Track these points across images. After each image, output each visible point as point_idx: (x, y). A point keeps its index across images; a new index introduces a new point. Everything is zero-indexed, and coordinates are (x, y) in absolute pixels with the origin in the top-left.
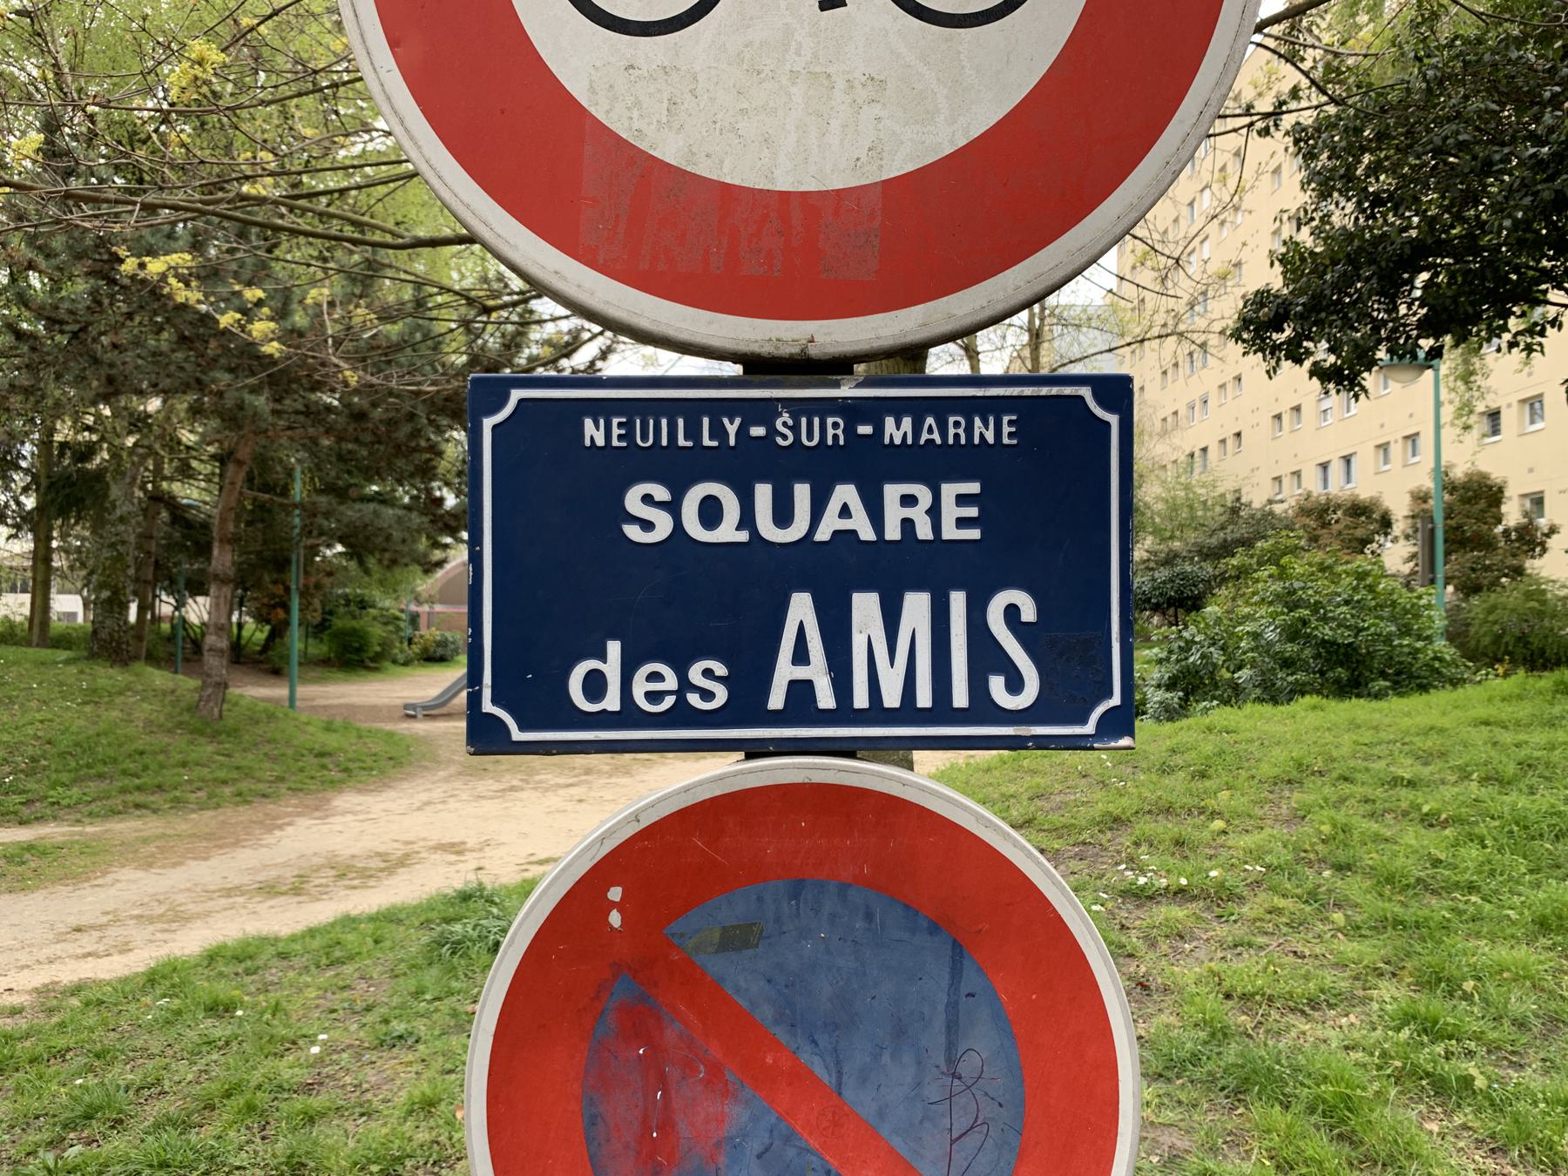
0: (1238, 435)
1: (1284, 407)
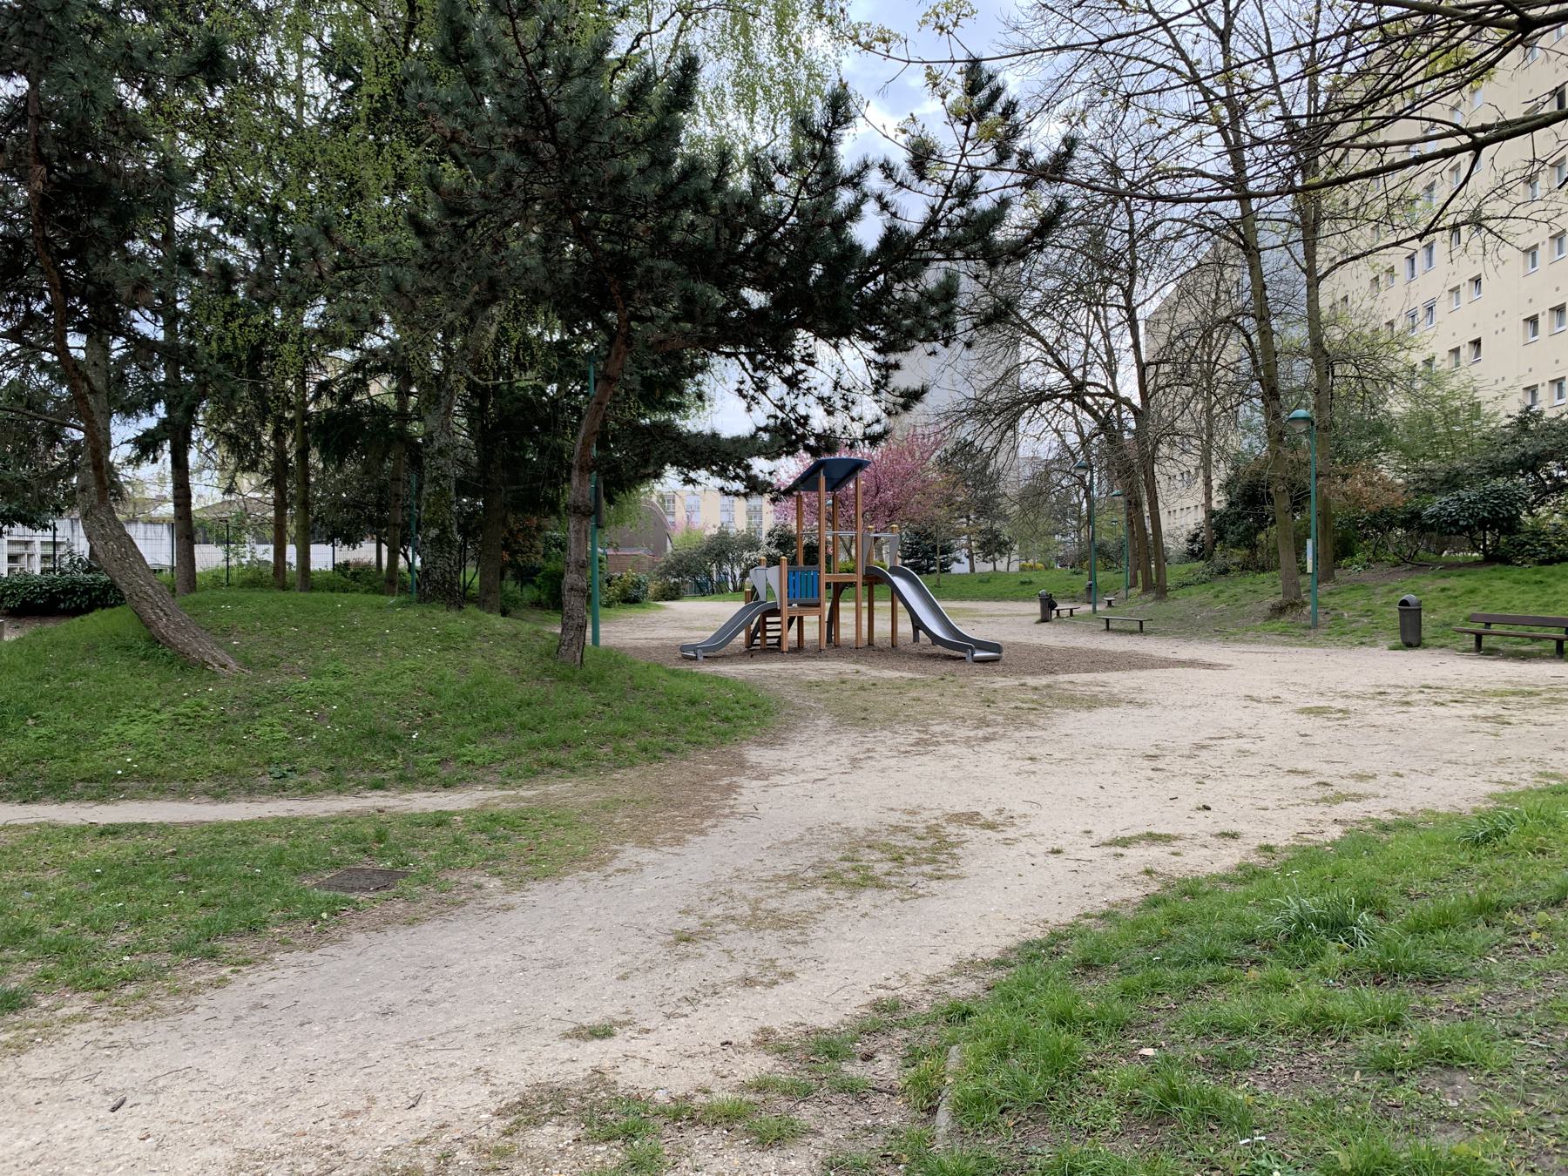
0: (1477, 343)
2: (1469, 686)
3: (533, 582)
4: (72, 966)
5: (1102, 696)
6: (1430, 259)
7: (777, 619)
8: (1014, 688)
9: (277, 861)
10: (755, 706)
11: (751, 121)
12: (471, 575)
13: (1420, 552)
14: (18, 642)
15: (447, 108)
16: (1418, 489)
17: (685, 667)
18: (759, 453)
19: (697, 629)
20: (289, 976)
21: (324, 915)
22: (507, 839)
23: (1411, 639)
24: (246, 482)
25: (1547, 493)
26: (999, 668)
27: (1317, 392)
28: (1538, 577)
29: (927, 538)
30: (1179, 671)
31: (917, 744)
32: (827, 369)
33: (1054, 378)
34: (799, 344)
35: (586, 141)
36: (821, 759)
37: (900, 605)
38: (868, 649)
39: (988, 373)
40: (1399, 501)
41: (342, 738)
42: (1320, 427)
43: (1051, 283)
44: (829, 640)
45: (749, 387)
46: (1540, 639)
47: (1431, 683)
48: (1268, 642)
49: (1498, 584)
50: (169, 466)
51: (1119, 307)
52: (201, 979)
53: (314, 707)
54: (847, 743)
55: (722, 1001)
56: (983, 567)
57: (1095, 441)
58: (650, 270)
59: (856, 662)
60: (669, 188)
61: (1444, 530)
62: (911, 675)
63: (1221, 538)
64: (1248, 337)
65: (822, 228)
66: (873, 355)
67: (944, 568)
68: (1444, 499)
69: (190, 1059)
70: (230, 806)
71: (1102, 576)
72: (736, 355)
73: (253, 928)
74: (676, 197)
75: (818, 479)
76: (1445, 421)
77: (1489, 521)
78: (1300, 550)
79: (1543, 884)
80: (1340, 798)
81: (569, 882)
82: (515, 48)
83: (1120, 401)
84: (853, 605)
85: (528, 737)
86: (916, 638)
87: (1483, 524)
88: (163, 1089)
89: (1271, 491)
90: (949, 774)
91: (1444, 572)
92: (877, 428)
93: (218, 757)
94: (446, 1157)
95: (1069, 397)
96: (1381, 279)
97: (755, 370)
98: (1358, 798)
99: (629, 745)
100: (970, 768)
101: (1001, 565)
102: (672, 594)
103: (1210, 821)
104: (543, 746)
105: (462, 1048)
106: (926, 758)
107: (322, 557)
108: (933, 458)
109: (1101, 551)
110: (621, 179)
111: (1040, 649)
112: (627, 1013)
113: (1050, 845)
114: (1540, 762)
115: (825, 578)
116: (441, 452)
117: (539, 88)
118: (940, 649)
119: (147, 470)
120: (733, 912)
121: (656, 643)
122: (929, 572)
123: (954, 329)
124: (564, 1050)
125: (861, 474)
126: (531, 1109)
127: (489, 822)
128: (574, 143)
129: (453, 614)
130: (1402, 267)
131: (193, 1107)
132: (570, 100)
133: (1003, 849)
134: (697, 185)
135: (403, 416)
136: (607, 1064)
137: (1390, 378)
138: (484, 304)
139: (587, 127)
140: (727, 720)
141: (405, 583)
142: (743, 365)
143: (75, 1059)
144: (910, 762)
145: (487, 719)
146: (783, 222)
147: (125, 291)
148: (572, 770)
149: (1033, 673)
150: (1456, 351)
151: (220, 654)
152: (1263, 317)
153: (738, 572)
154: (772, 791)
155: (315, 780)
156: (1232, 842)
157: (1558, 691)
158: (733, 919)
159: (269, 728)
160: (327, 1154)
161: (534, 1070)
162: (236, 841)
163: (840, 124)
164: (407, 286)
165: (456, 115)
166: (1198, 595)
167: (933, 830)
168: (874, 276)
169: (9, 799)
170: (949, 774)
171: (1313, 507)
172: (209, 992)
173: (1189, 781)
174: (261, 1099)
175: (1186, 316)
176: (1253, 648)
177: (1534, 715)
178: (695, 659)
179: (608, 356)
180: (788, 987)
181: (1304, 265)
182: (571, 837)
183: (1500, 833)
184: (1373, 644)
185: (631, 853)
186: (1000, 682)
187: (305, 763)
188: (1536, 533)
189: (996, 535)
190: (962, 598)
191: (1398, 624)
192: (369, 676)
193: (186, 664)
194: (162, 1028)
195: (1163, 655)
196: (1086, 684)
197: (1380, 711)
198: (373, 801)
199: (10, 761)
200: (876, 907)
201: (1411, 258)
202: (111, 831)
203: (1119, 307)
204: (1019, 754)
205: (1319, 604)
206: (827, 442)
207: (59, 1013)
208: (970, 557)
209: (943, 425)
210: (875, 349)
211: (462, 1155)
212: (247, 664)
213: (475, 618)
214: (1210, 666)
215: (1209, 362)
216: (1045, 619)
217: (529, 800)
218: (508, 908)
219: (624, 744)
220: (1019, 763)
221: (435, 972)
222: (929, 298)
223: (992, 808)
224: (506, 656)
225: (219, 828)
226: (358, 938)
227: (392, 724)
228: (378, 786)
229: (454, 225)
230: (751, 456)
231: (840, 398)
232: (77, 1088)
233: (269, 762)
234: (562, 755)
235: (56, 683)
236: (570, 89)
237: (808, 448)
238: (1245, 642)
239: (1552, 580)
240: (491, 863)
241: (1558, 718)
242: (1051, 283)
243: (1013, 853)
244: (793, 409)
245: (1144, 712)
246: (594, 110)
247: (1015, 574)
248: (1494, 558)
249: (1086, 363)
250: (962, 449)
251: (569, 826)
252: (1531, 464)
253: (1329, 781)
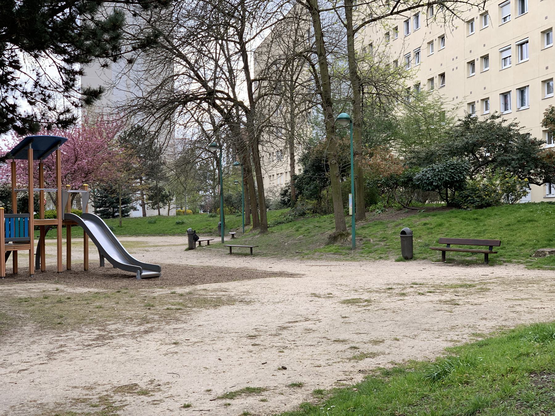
0: (443, 76)
1: (476, 56)
2: (438, 282)
5: (224, 298)
6: (417, 23)
8: (167, 296)
13: (413, 202)
16: (411, 163)
23: (406, 255)
25: (480, 166)
26: (158, 282)
27: (354, 102)
28: (475, 216)
29: (112, 193)
30: (273, 280)
31: (97, 339)
33: (195, 86)
34: (7, 54)
36: (25, 355)
37: (90, 240)
38: (67, 273)
39: (152, 81)
40: (399, 170)
42: (357, 124)
43: (191, 23)
44: (37, 267)
46: (474, 253)
47: (417, 281)
48: (327, 259)
49: (454, 220)
51: (235, 42)
54: (45, 343)
56: (152, 213)
57: (222, 129)
59: (56, 283)
61: (426, 188)
62: (96, 290)
63: (300, 193)
64: (313, 66)
67: (125, 213)
68: (425, 169)
71: (228, 218)
76: (426, 121)
77: (449, 183)
78: (345, 201)
79: (465, 403)
80: (363, 356)
83: (239, 105)
84: (56, 241)
86: (102, 263)
87: (447, 184)
89: (329, 163)
90: (119, 359)
91: (426, 214)
95: (205, 99)
96: (435, 43)
98: (373, 355)
100: (133, 353)
101: (164, 212)
103: (286, 376)
106: (102, 349)
108: (116, 138)
109: (228, 201)
111: (186, 268)
113: (183, 402)
114: (474, 327)
115: (34, 222)
118: (118, 271)
122: (114, 217)
123: (120, 50)
130: (402, 27)
133: (152, 408)
137: (396, 95)
144: (91, 352)
149: (181, 285)
150: (432, 80)
152: (322, 54)
156: (299, 390)
157: (485, 284)
166: (287, 229)
167: (103, 400)
170: (119, 359)
171: (352, 173)
173: (275, 351)
175: (278, 51)
176: (319, 263)
177: (471, 299)
181: (346, 22)
183: (445, 373)
184: (387, 258)
186: (158, 292)
188: (474, 190)
189: (160, 190)
190: (137, 234)
191: (400, 245)
195: (264, 269)
196: (215, 291)
197: (388, 300)
201: (407, 22)
203: (235, 42)
204: (167, 341)
205: (356, 234)
206: (30, 124)
208: (143, 205)
209: (122, 114)
210: (64, 60)
214: (292, 275)
215: (292, 81)
216: (191, 248)
220: (167, 347)
222: (102, 27)
223: (146, 380)
231: (40, 93)
237: (16, 128)
238: (314, 259)
239: (482, 217)
241: (484, 300)
242: (191, 23)
243: (158, 410)
245: (249, 307)
247: (173, 217)
248: (453, 205)
249: (216, 78)
250: (135, 132)
252: (471, 148)
253: (357, 345)
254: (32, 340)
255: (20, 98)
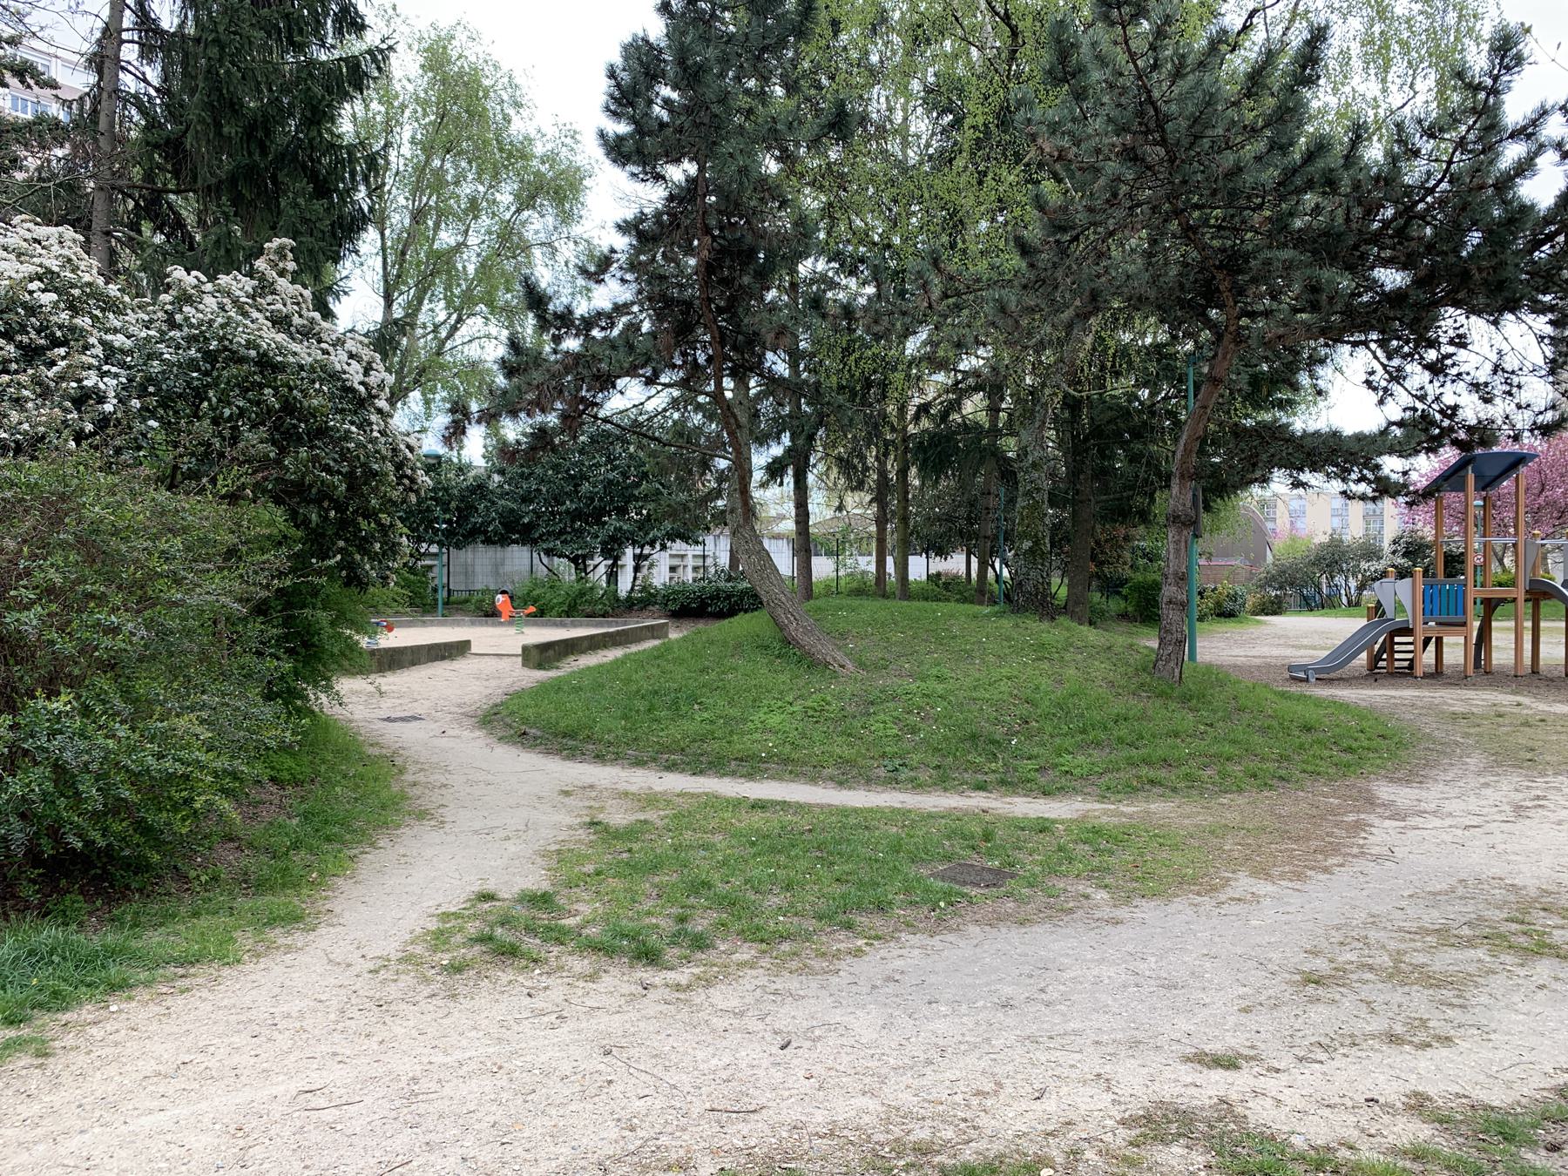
3: (1119, 593)
4: (740, 918)
7: (1410, 639)
9: (896, 848)
10: (1383, 737)
11: (1384, 81)
12: (1059, 587)
14: (684, 639)
15: (1054, 128)
17: (1295, 689)
18: (1391, 451)
19: (1306, 647)
20: (910, 954)
21: (942, 904)
22: (1111, 853)
24: (851, 499)
32: (1486, 351)
35: (1197, 137)
36: (1473, 803)
38: (1532, 676)
41: (946, 739)
44: (1477, 665)
45: (1380, 377)
50: (792, 485)
52: (842, 946)
53: (921, 708)
54: (1507, 788)
55: (1364, 1054)
58: (1267, 262)
60: (1291, 173)
65: (1480, 192)
66: (1549, 330)
69: (837, 1016)
70: (851, 793)
72: (1365, 343)
73: (881, 907)
74: (1298, 181)
75: (1465, 478)
81: (1178, 904)
82: (1126, 56)
84: (1512, 624)
85: (1127, 752)
88: (819, 1038)
92: (1549, 417)
93: (841, 748)
94: (1075, 1153)
97: (1389, 358)
99: (1235, 769)
102: (1274, 608)
104: (1144, 766)
105: (1080, 1051)
107: (918, 567)
110: (1238, 170)
112: (1252, 1047)
116: (1034, 465)
117: (1149, 92)
119: (773, 491)
120: (1370, 961)
121: (1258, 661)
124: (1187, 1073)
125: (1523, 470)
126: (1160, 1124)
127: (1093, 834)
128: (1185, 142)
129: (1045, 625)
131: (845, 1059)
132: (1182, 99)
134: (1324, 168)
135: (995, 432)
136: (1234, 1096)
138: (1083, 316)
139: (1199, 123)
140: (1349, 750)
141: (991, 593)
142: (1374, 353)
143: (749, 999)
145: (1084, 731)
146: (1431, 191)
147: (769, 338)
148: (1174, 790)
151: (839, 656)
153: (1353, 584)
154: (1411, 833)
155: (923, 776)
158: (1371, 968)
159: (881, 724)
160: (963, 1125)
161: (1156, 1086)
162: (858, 826)
163: (1508, 68)
164: (1012, 306)
165: (1063, 133)
168: (1550, 238)
169: (683, 771)
172: (849, 959)
174: (900, 1063)
178: (1307, 680)
179: (1216, 355)
180: (1444, 1052)
182: (1178, 859)
185: (1244, 883)
187: (915, 758)
192: (968, 682)
193: (812, 663)
194: (814, 985)
198: (976, 801)
199: (683, 738)
200: (1557, 979)
202: (759, 805)
206: (1483, 433)
207: (733, 957)
210: (1551, 322)
211: (1090, 1154)
212: (861, 665)
213: (1068, 629)
217: (1131, 816)
218: (1117, 922)
219: (1230, 767)
221: (1048, 974)
224: (1100, 668)
225: (845, 812)
226: (973, 930)
227: (992, 729)
228: (981, 787)
229: (1057, 242)
230: (1381, 454)
232: (752, 1024)
233: (884, 755)
234: (1162, 774)
235: (713, 675)
236: (1183, 85)
237: (1456, 443)
240: (1098, 874)
244: (1437, 399)
246: (1208, 104)
251: (1175, 848)
254: (1482, 780)
255: (1465, 394)
